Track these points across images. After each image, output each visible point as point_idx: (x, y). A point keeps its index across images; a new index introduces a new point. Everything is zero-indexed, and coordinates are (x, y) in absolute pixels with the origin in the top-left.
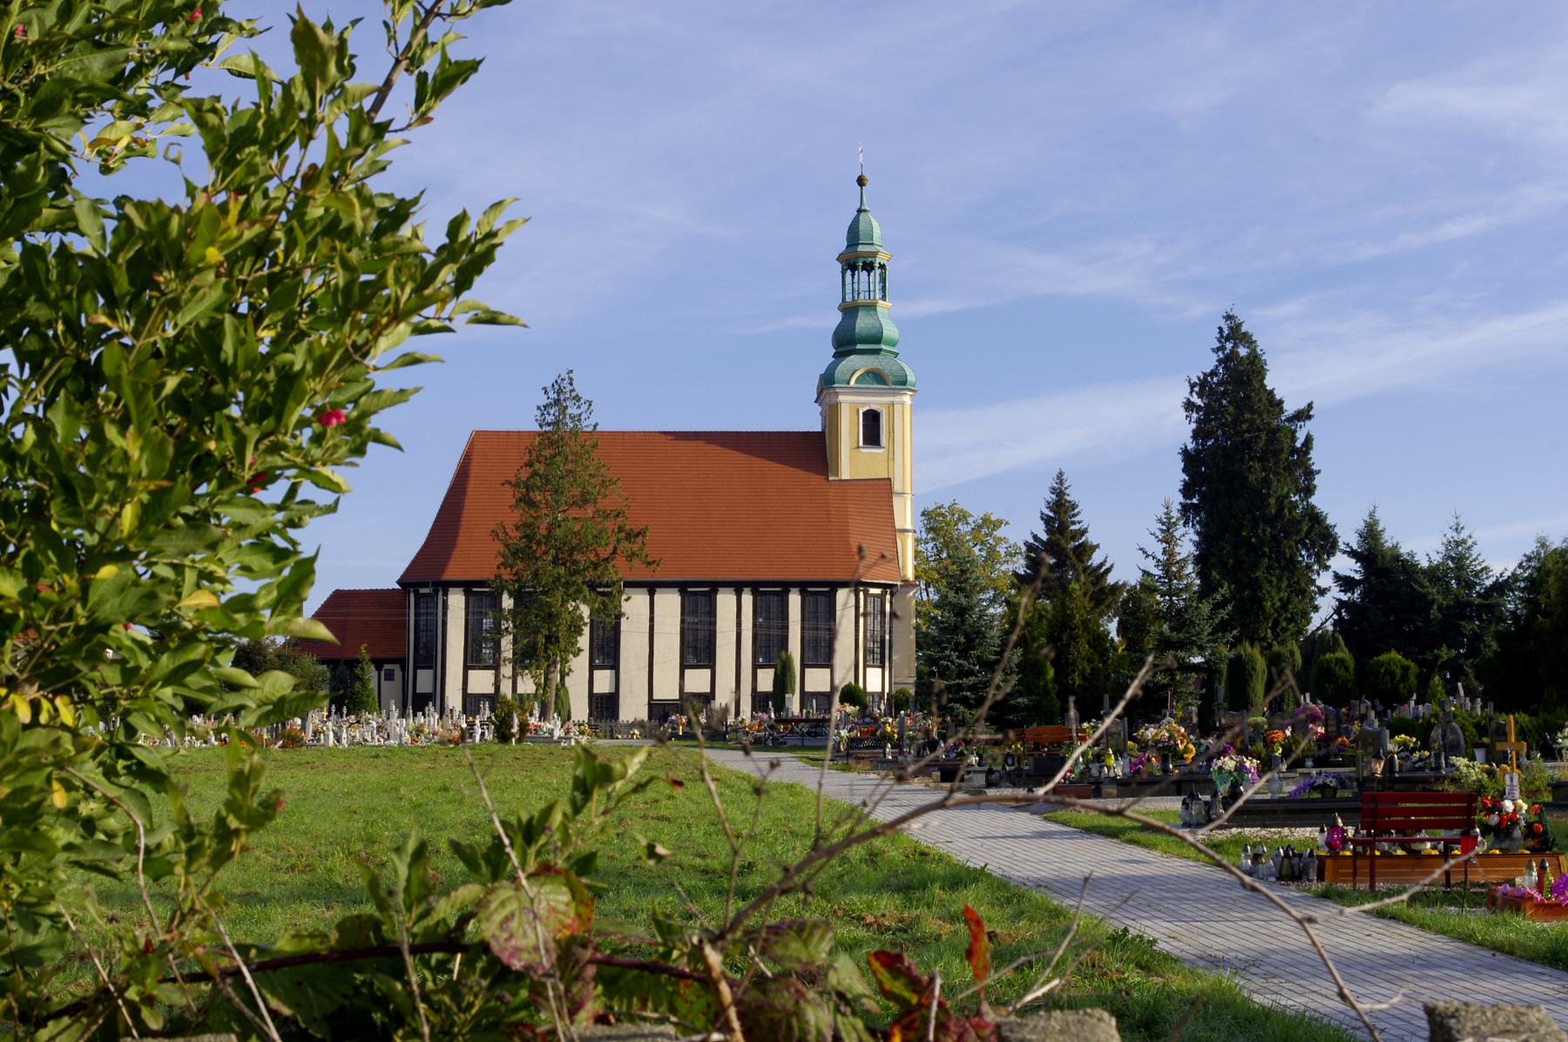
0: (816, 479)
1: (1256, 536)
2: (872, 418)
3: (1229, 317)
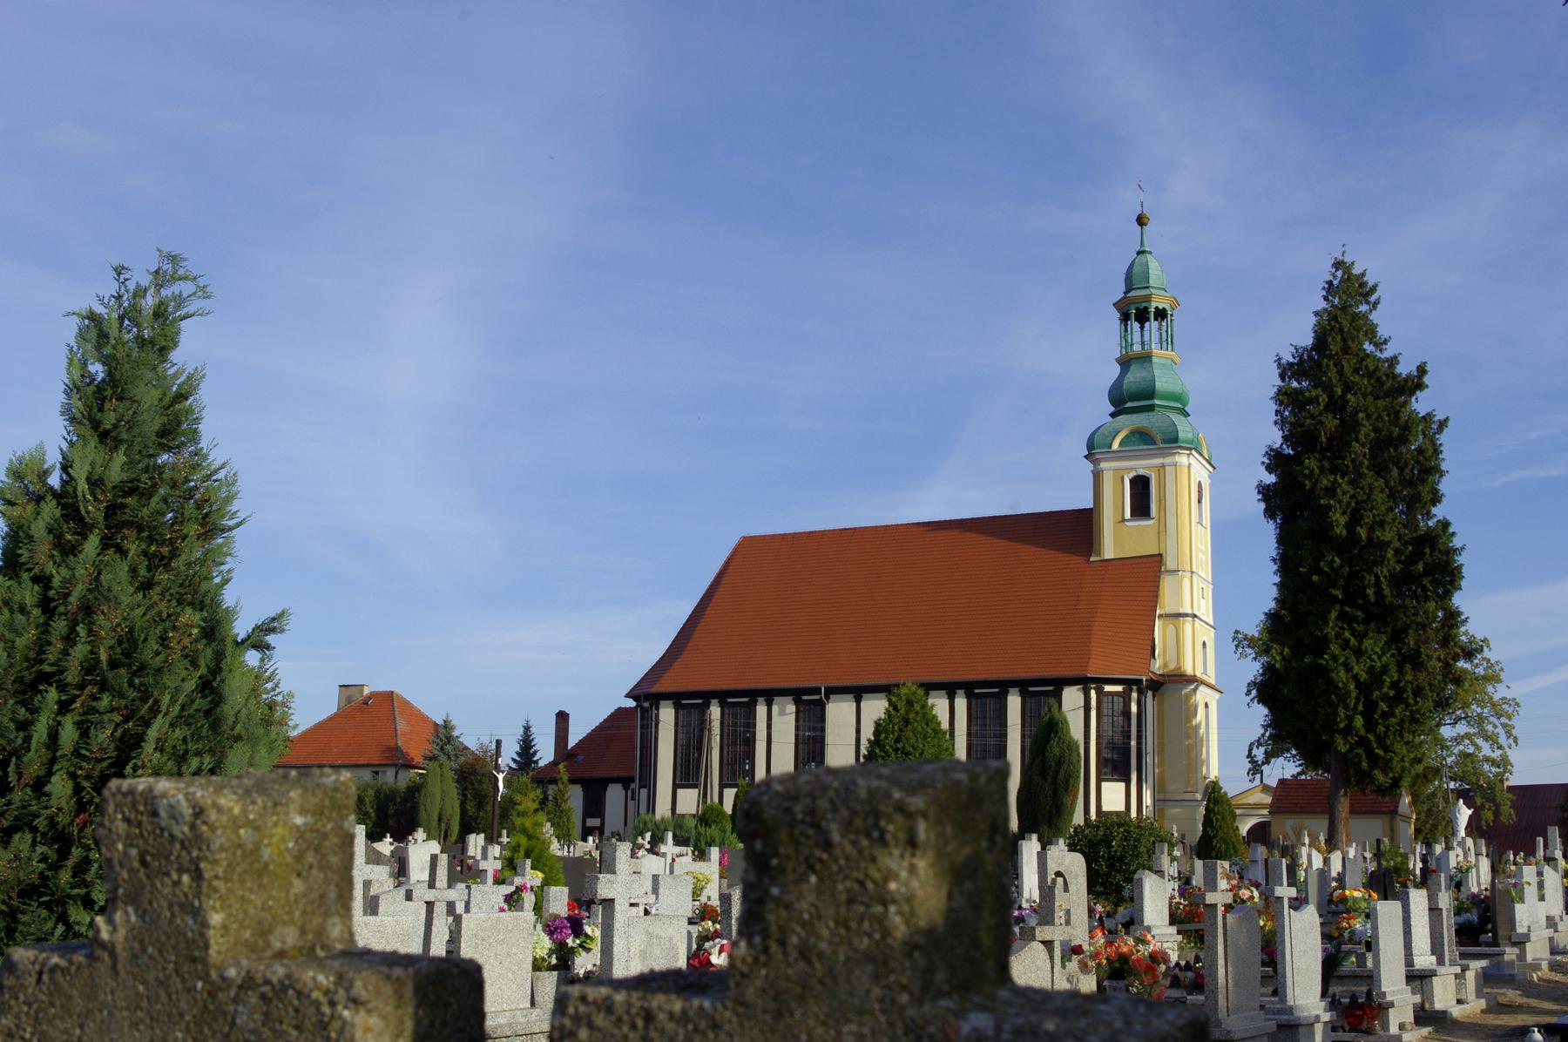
0: (1076, 561)
1: (1320, 572)
2: (1141, 486)
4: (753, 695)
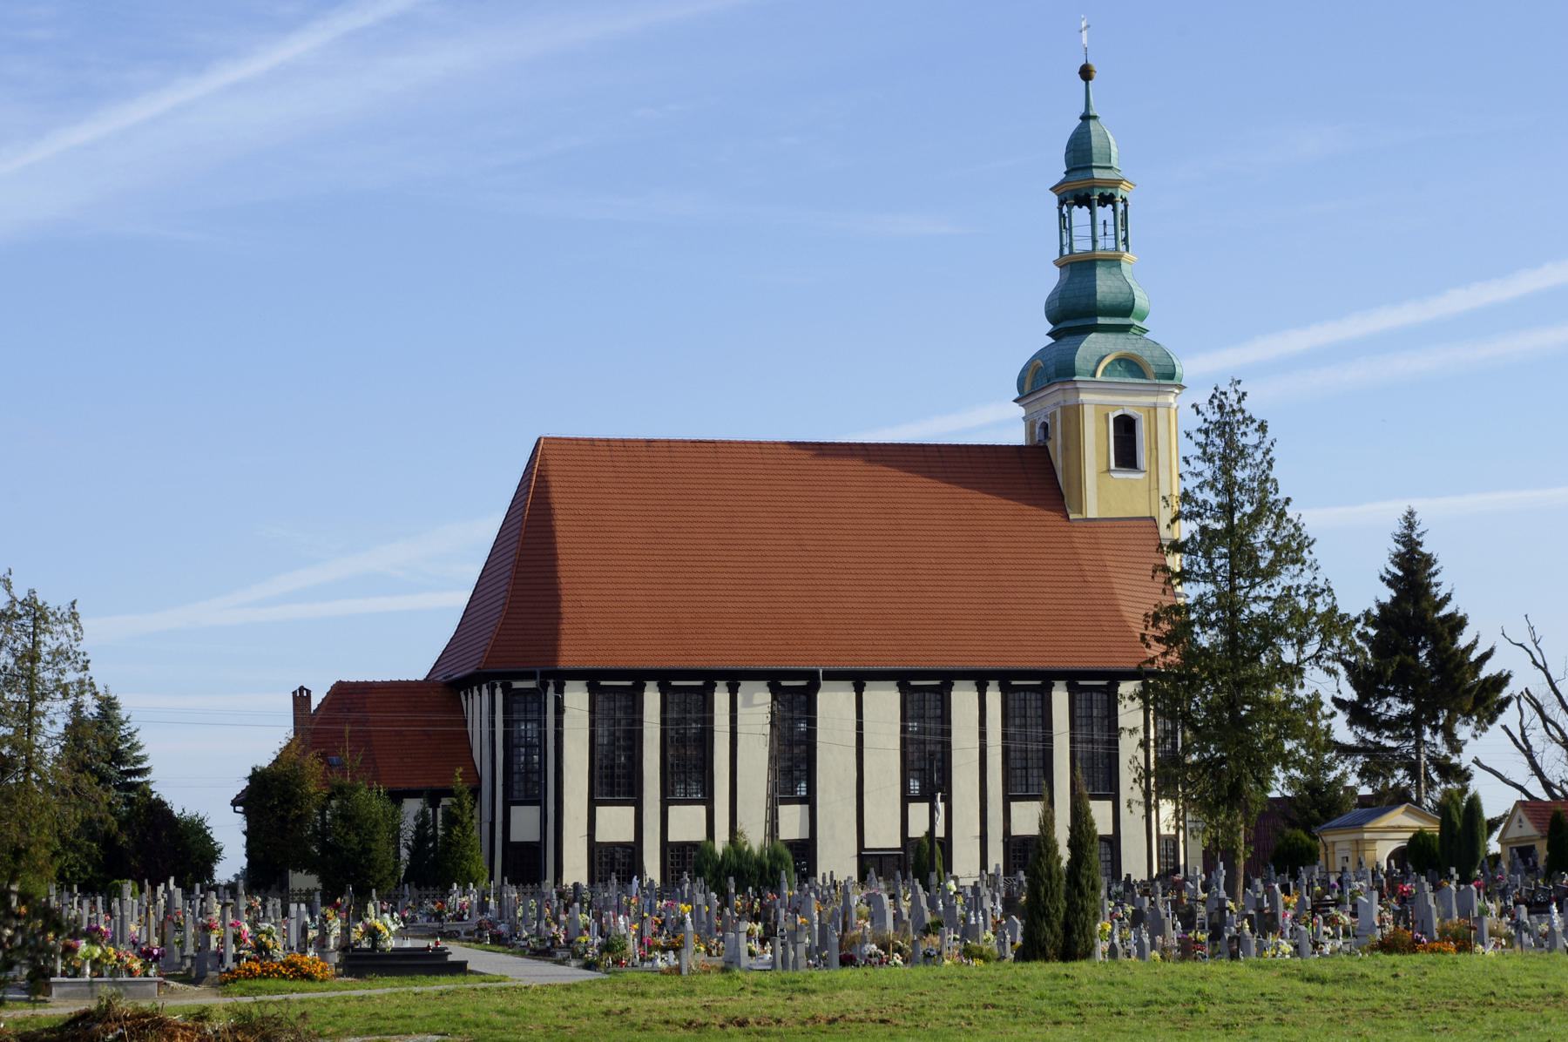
0: (1052, 517)
2: (1126, 428)
4: (710, 677)
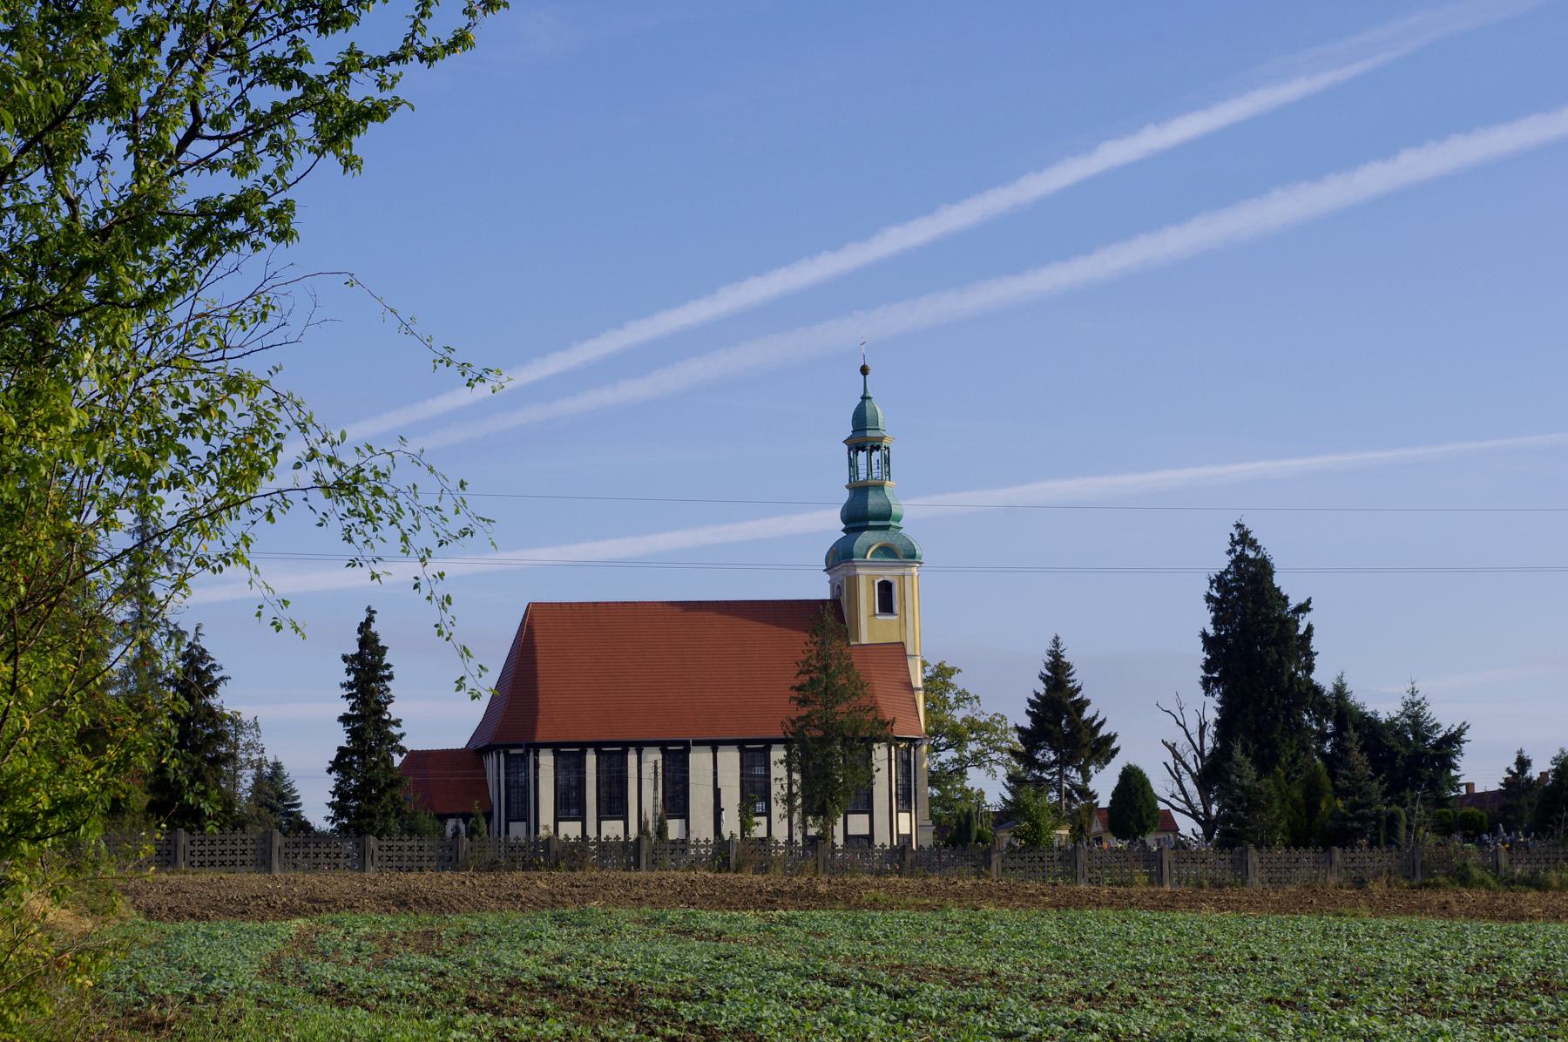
2: (886, 589)
3: (1239, 526)
4: (626, 745)
